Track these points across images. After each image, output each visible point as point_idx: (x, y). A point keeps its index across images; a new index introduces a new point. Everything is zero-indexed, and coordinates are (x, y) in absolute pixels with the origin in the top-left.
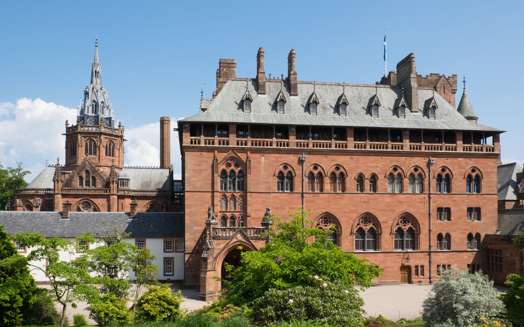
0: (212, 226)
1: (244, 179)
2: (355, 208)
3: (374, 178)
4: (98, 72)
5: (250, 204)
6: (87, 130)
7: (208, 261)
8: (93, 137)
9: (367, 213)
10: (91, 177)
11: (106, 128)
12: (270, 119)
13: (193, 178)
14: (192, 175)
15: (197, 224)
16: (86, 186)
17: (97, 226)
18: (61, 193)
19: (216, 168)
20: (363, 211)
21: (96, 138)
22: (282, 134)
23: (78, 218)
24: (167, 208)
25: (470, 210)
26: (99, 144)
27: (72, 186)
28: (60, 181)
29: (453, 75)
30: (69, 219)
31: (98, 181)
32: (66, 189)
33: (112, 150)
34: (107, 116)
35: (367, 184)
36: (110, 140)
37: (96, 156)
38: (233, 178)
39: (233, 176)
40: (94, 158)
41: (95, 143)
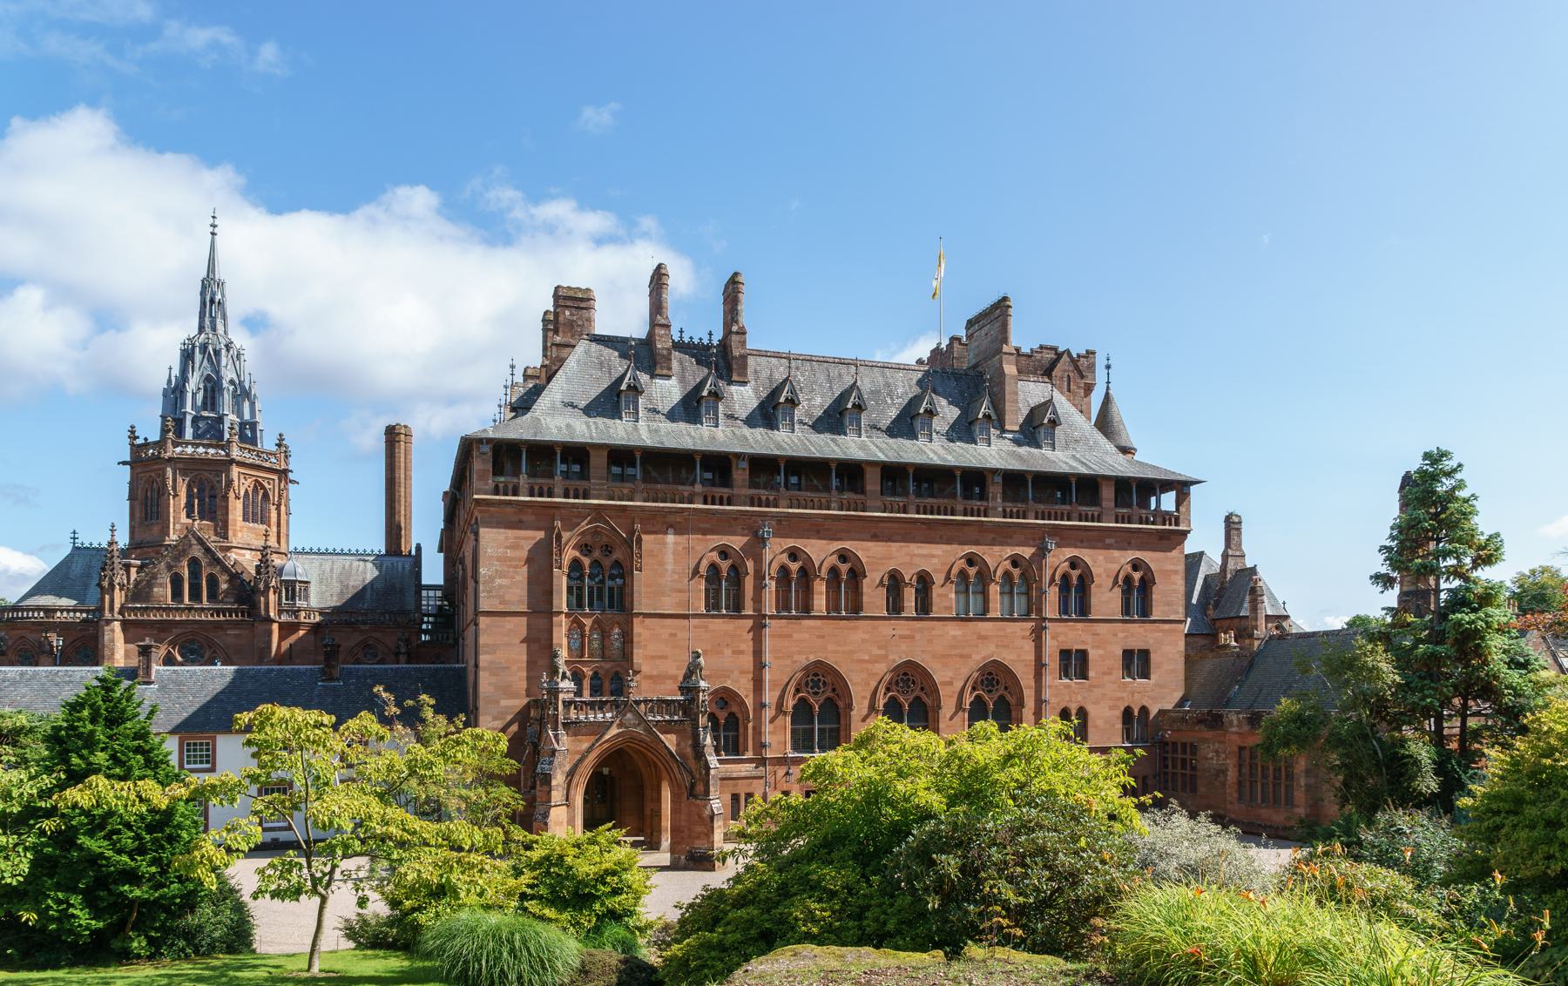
0: (561, 696)
1: (624, 583)
2: (883, 652)
3: (924, 581)
5: (639, 642)
7: (554, 783)
9: (909, 662)
12: (687, 438)
15: (508, 692)
20: (900, 658)
22: (713, 475)
24: (408, 654)
25: (1128, 654)
29: (1087, 351)
35: (910, 598)
38: (597, 580)
39: (598, 575)
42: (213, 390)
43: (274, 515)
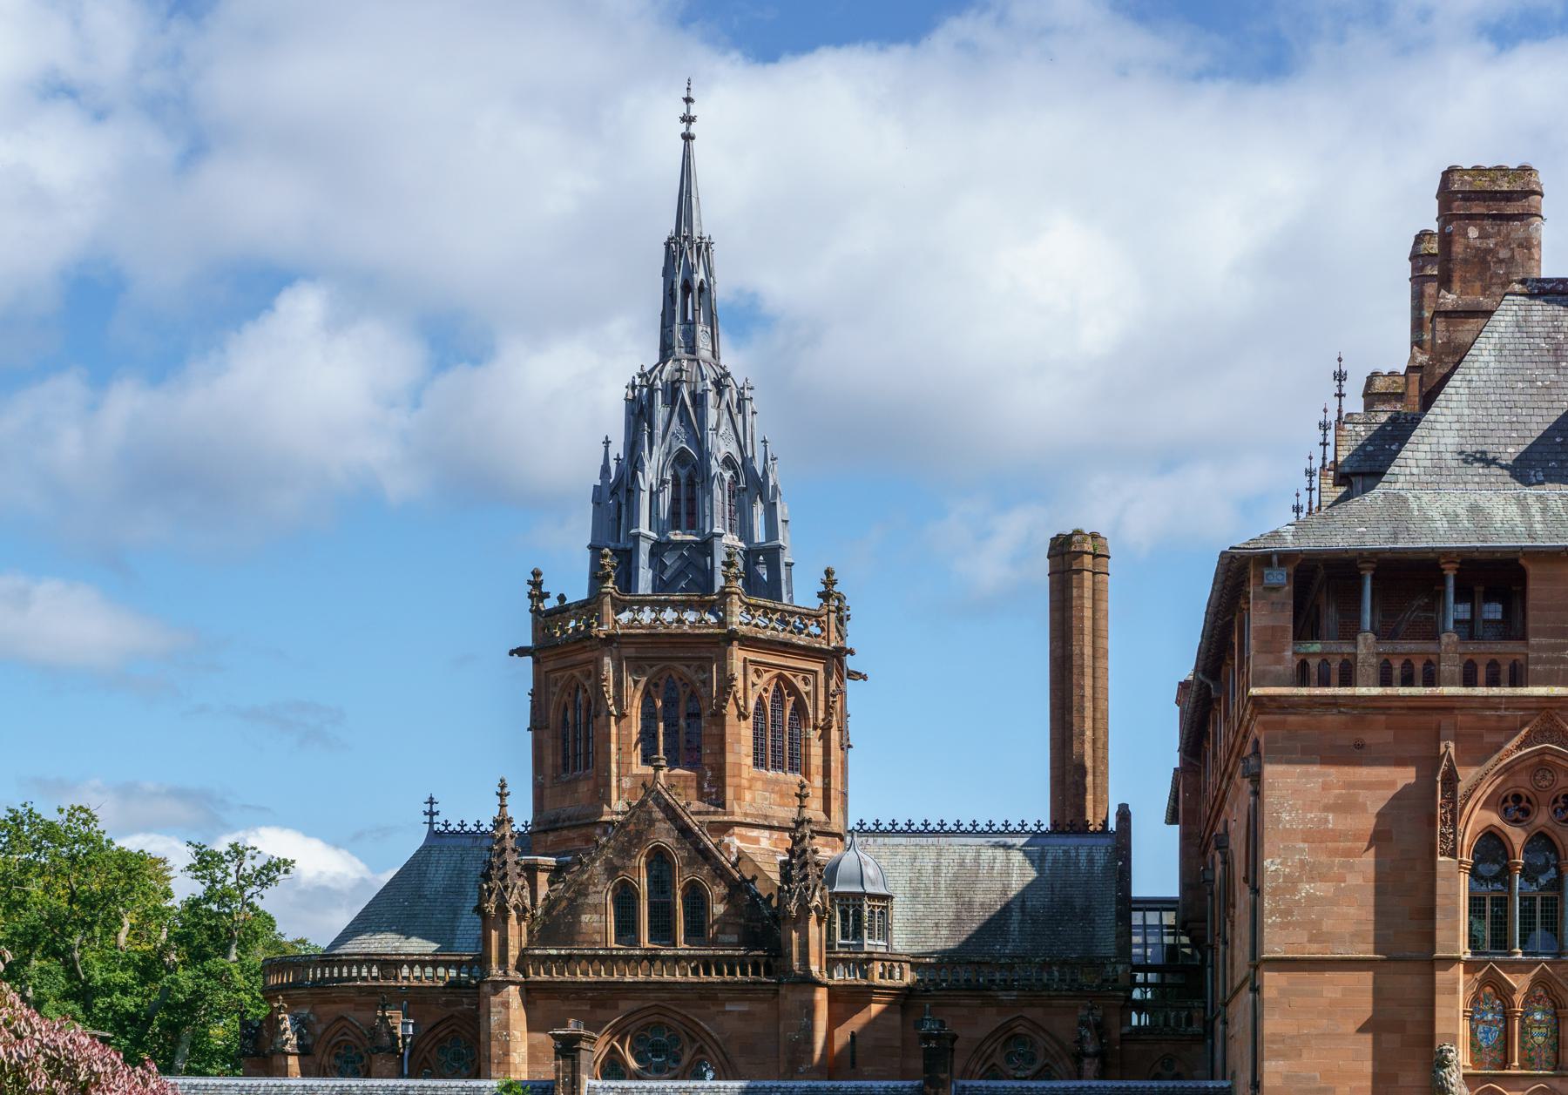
6: (650, 627)
13: (1311, 879)
14: (1303, 863)
19: (1444, 823)
24: (1101, 1055)
28: (513, 913)
42: (691, 483)
43: (816, 750)
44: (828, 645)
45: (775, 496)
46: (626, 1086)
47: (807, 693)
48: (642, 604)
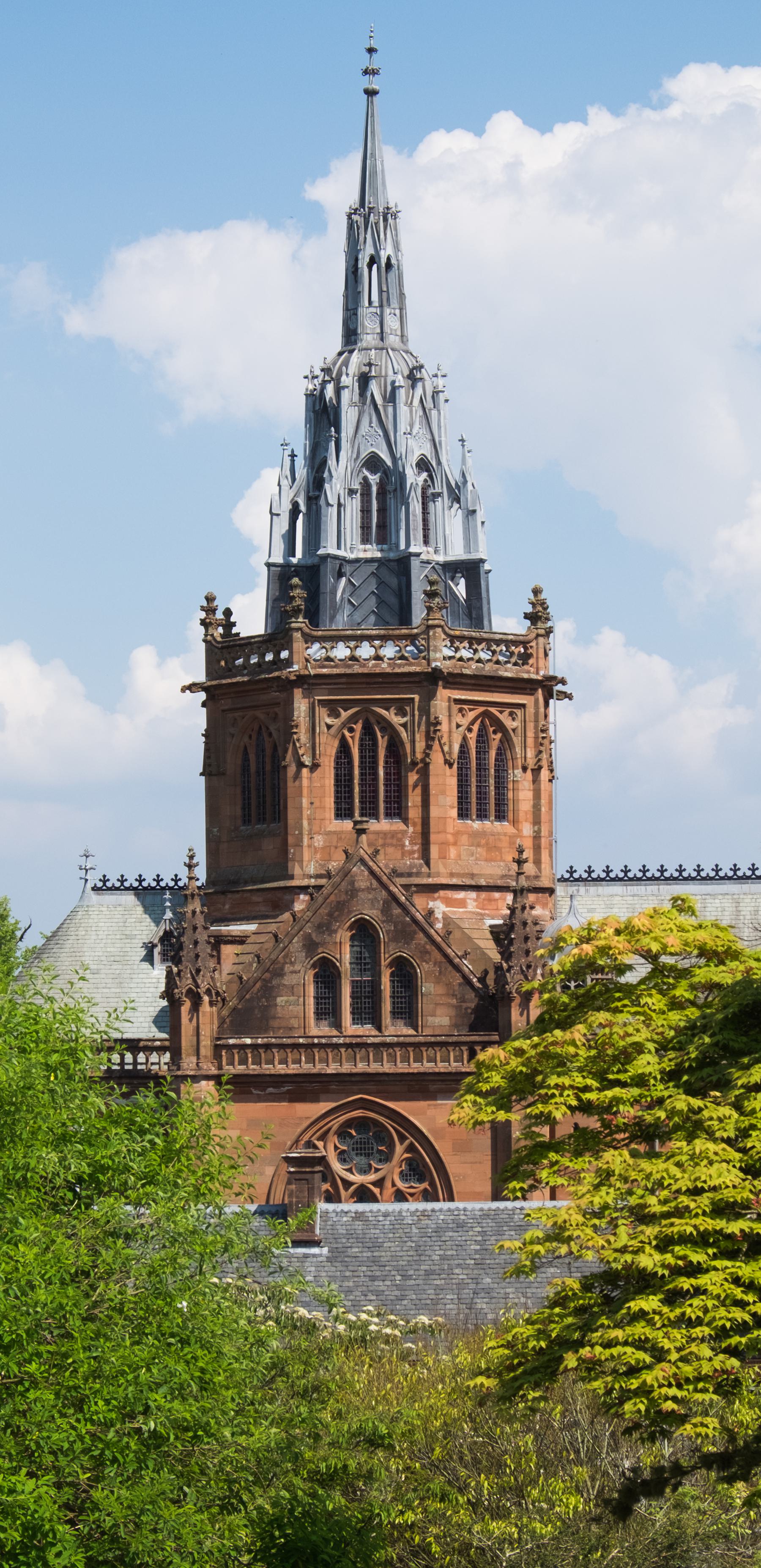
4: (389, 265)
8: (386, 704)
10: (390, 965)
11: (462, 638)
16: (355, 1021)
17: (488, 1291)
18: (214, 1071)
21: (402, 712)
23: (376, 1245)
26: (420, 745)
27: (275, 1023)
28: (206, 998)
30: (325, 1251)
31: (427, 987)
32: (244, 1047)
33: (497, 777)
34: (457, 552)
36: (486, 714)
37: (405, 821)
40: (393, 834)
41: (395, 748)
44: (537, 673)
45: (474, 503)
46: (360, 1210)
47: (514, 730)
48: (336, 639)
